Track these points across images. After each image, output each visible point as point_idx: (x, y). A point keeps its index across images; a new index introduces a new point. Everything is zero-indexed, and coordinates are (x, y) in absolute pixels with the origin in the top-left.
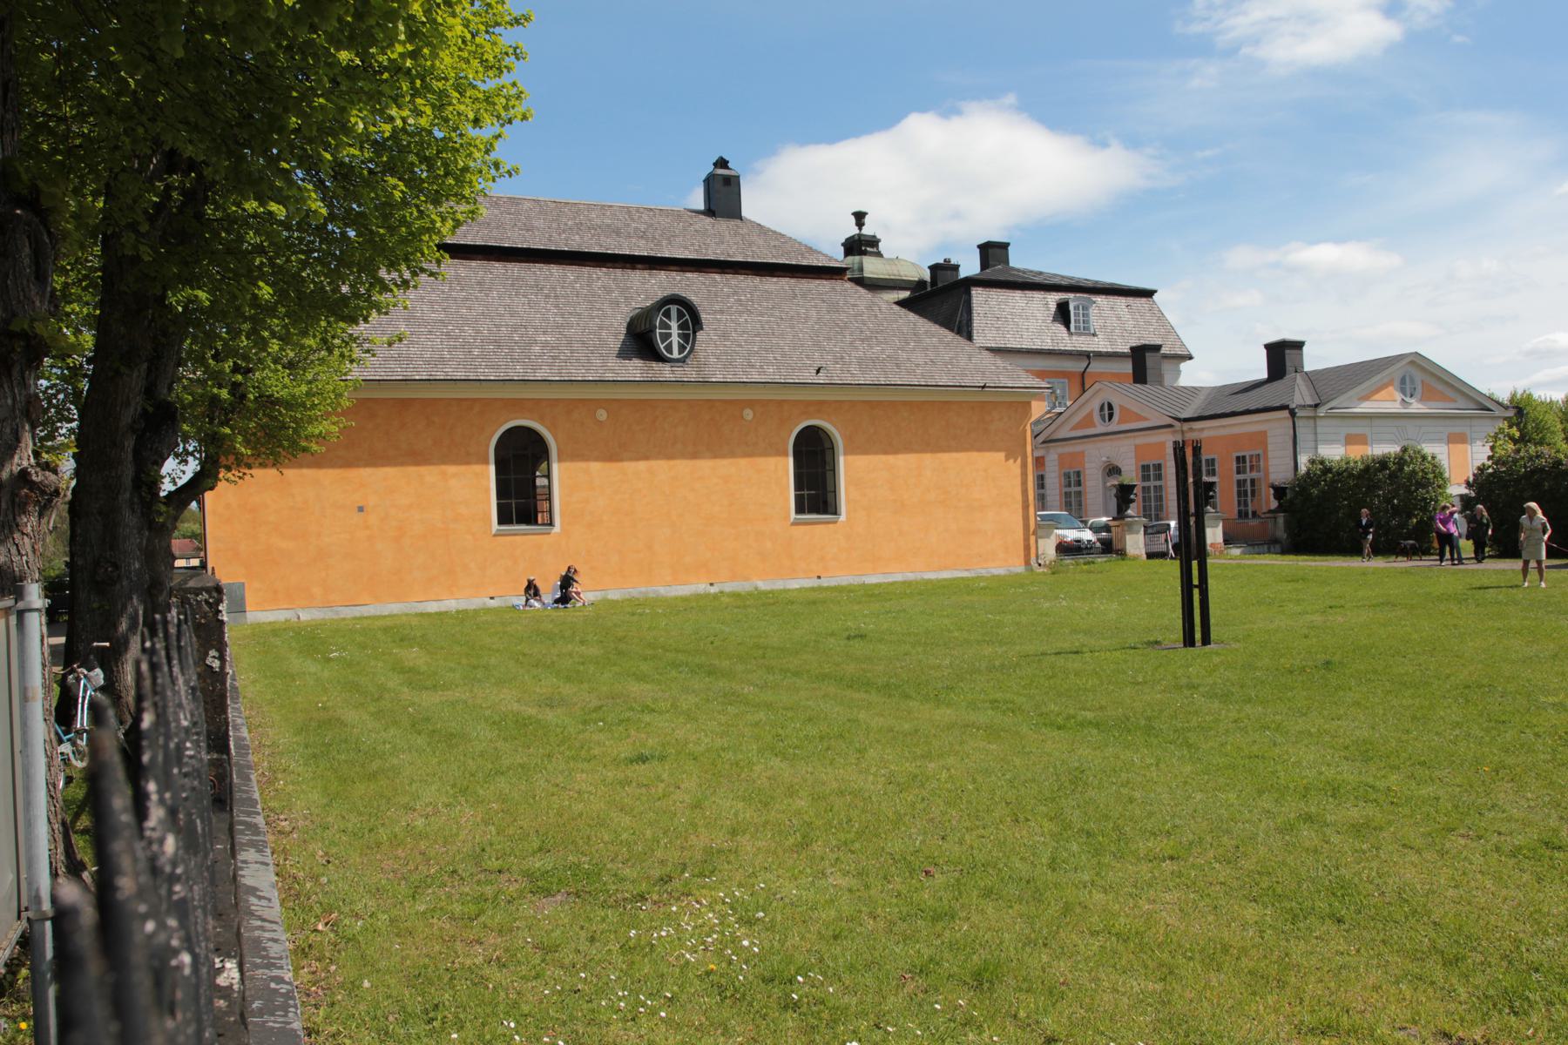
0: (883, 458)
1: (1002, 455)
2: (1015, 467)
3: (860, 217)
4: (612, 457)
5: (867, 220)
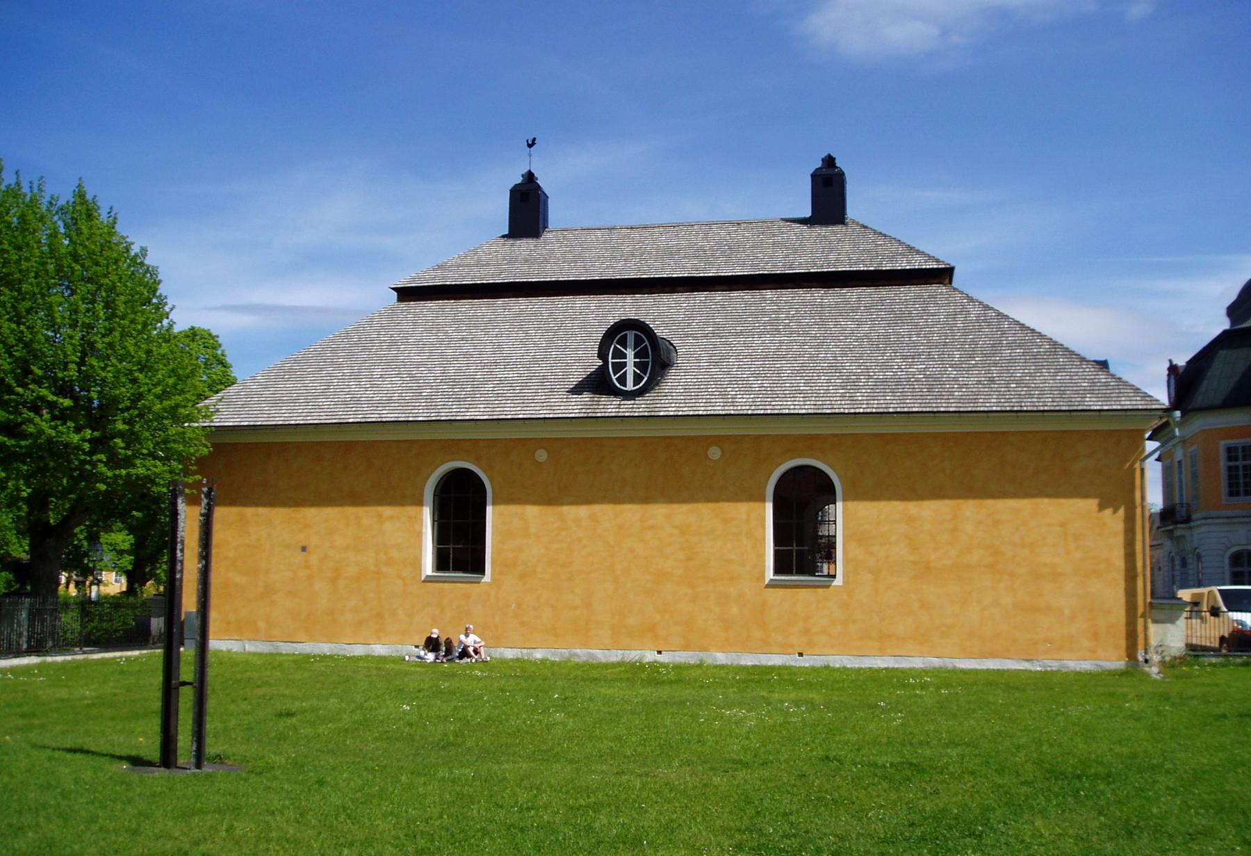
1: (1092, 503)
4: (550, 498)
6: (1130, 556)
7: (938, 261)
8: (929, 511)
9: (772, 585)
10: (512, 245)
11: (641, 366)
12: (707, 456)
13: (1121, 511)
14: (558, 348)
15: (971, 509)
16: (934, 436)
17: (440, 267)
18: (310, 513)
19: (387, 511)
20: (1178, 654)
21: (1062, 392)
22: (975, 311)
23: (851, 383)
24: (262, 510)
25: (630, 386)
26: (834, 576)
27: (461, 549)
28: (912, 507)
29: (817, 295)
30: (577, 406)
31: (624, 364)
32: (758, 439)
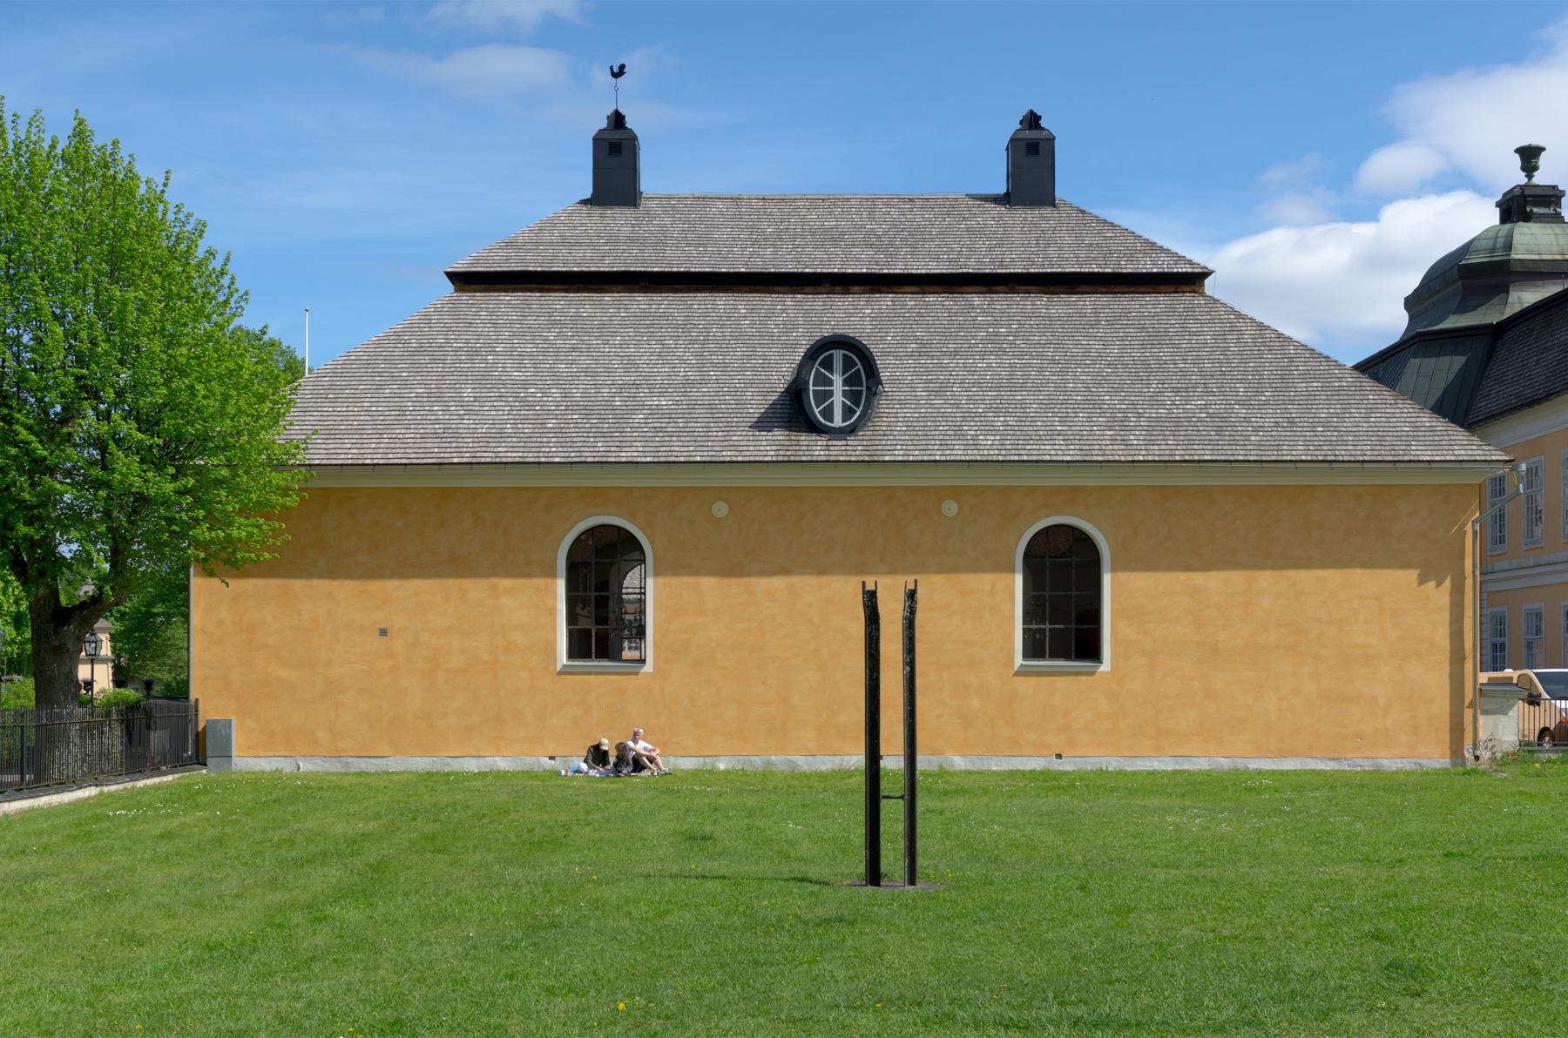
0: (1183, 576)
1: (1412, 575)
2: (1439, 595)
3: (1529, 156)
4: (732, 568)
5: (1543, 160)
6: (1457, 635)
7: (1190, 262)
8: (1215, 582)
9: (1022, 673)
10: (603, 216)
11: (854, 397)
12: (940, 512)
13: (1447, 583)
14: (714, 365)
15: (1266, 579)
16: (1225, 490)
17: (509, 244)
18: (391, 585)
19: (505, 583)
20: (1511, 750)
21: (1381, 439)
22: (1249, 332)
23: (1119, 423)
24: (320, 584)
25: (838, 421)
26: (642, 661)
27: (602, 629)
28: (1198, 578)
29: (1039, 304)
30: (772, 445)
31: (830, 394)
32: (1004, 491)
